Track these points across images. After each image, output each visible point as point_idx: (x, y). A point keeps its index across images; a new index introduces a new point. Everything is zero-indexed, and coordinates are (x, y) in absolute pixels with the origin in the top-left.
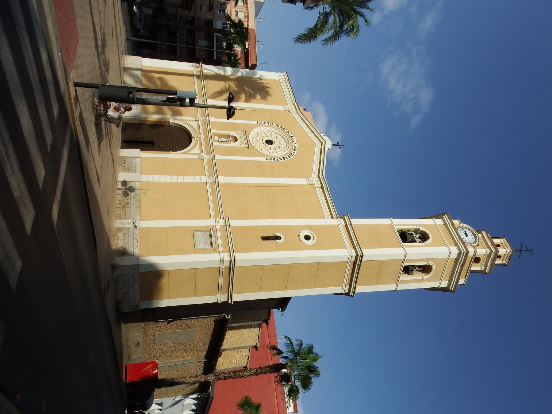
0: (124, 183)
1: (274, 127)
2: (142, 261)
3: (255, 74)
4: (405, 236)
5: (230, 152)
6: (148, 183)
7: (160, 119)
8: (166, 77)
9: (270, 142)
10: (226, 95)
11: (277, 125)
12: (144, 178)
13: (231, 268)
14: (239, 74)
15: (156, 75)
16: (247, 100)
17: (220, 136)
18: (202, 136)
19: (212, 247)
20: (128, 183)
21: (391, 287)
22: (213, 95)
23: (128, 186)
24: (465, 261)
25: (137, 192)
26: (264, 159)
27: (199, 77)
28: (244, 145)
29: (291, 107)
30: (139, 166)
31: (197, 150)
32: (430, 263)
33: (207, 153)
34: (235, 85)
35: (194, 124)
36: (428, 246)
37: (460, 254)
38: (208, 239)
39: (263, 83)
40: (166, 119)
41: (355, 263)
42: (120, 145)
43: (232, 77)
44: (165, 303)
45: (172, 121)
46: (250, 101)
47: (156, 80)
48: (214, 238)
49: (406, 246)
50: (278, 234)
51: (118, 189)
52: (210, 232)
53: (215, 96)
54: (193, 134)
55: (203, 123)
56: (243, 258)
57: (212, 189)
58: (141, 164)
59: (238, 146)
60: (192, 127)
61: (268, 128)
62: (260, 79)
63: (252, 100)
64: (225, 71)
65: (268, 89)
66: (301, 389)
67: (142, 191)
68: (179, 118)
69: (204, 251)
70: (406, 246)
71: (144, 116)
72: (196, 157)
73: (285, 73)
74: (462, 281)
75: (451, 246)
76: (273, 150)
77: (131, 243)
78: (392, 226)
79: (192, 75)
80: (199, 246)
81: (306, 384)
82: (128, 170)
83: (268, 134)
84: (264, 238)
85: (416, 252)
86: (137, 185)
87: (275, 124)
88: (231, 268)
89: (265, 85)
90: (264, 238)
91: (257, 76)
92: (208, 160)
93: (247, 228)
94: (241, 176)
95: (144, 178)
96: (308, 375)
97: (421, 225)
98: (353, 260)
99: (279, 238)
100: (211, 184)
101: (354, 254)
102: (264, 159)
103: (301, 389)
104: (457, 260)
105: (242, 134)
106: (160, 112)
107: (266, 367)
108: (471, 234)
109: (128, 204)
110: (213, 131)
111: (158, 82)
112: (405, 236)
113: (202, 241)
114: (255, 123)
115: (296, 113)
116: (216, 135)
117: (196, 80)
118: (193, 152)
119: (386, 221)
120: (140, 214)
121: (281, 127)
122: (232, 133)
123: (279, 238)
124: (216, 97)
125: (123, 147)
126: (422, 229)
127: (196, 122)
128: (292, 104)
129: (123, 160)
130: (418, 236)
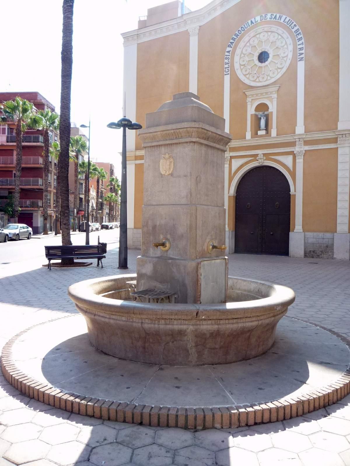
11: (229, 46)
31: (288, 160)
35: (236, 164)
59: (275, 103)
72: (300, 161)
114: (227, 79)
127: (233, 160)
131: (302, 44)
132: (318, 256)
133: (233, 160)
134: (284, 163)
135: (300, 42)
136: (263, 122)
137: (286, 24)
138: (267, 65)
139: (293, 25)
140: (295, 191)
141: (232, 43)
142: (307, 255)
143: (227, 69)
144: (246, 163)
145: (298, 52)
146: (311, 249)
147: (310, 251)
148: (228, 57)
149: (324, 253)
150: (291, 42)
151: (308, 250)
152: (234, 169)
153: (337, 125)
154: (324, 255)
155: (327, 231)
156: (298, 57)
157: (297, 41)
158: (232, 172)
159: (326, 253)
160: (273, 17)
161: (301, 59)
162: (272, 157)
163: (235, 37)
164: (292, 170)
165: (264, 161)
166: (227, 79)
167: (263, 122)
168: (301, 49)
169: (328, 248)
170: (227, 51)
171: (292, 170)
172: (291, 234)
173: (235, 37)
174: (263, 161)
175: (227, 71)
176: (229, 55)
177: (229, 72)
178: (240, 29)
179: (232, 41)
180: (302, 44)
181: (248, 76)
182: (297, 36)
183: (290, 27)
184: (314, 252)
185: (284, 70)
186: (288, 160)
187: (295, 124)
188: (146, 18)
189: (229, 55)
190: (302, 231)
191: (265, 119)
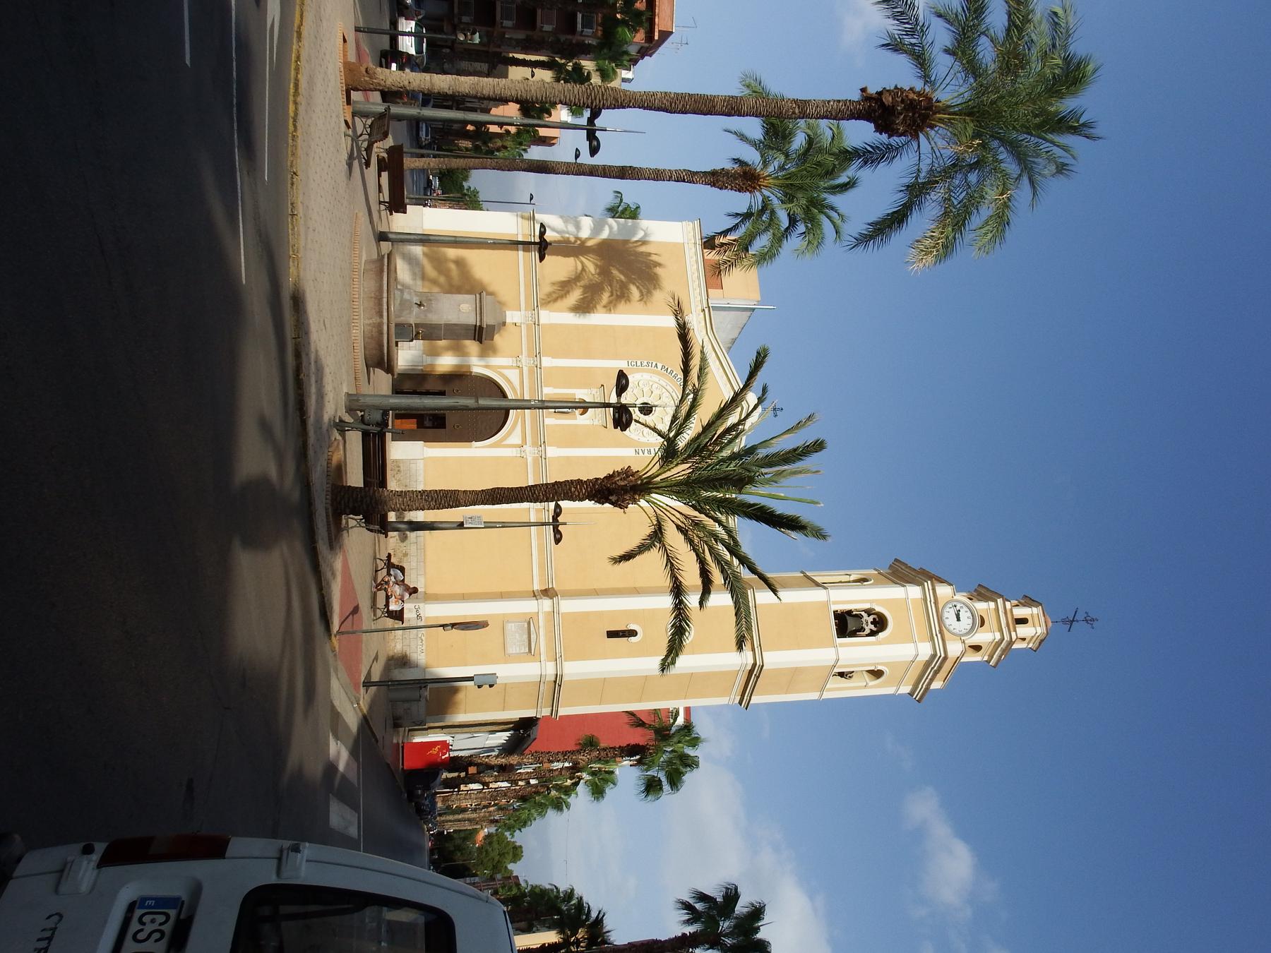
1: (659, 374)
2: (431, 673)
3: (634, 230)
4: (846, 624)
7: (456, 366)
10: (575, 296)
13: (557, 682)
14: (605, 234)
15: (452, 253)
16: (609, 307)
19: (530, 652)
21: (814, 696)
22: (549, 295)
24: (940, 668)
31: (516, 438)
32: (880, 668)
33: (534, 444)
34: (596, 265)
35: (513, 375)
36: (880, 643)
37: (934, 656)
38: (526, 636)
41: (751, 672)
43: (590, 243)
44: (461, 718)
47: (453, 266)
48: (533, 637)
49: (841, 645)
50: (632, 627)
52: (529, 622)
55: (531, 371)
56: (574, 669)
59: (587, 422)
60: (509, 381)
62: (643, 242)
63: (622, 306)
64: (578, 227)
65: (658, 270)
66: (666, 787)
69: (517, 659)
70: (841, 645)
71: (428, 360)
73: (697, 223)
74: (937, 685)
75: (922, 641)
77: (413, 647)
78: (827, 603)
80: (512, 650)
81: (675, 780)
83: (656, 392)
84: (611, 634)
85: (858, 652)
87: (660, 366)
88: (557, 682)
89: (654, 258)
90: (611, 634)
91: (640, 235)
92: (535, 460)
93: (586, 615)
94: (603, 358)
96: (678, 769)
97: (877, 601)
98: (749, 668)
99: (633, 633)
101: (751, 661)
103: (666, 787)
104: (928, 664)
106: (459, 351)
107: (614, 748)
108: (969, 614)
109: (406, 555)
112: (846, 624)
113: (516, 644)
118: (508, 442)
119: (817, 595)
120: (425, 574)
121: (671, 372)
123: (633, 633)
124: (555, 300)
126: (878, 609)
127: (517, 371)
128: (700, 308)
130: (871, 619)
133: (517, 371)
152: (506, 372)
186: (516, 438)
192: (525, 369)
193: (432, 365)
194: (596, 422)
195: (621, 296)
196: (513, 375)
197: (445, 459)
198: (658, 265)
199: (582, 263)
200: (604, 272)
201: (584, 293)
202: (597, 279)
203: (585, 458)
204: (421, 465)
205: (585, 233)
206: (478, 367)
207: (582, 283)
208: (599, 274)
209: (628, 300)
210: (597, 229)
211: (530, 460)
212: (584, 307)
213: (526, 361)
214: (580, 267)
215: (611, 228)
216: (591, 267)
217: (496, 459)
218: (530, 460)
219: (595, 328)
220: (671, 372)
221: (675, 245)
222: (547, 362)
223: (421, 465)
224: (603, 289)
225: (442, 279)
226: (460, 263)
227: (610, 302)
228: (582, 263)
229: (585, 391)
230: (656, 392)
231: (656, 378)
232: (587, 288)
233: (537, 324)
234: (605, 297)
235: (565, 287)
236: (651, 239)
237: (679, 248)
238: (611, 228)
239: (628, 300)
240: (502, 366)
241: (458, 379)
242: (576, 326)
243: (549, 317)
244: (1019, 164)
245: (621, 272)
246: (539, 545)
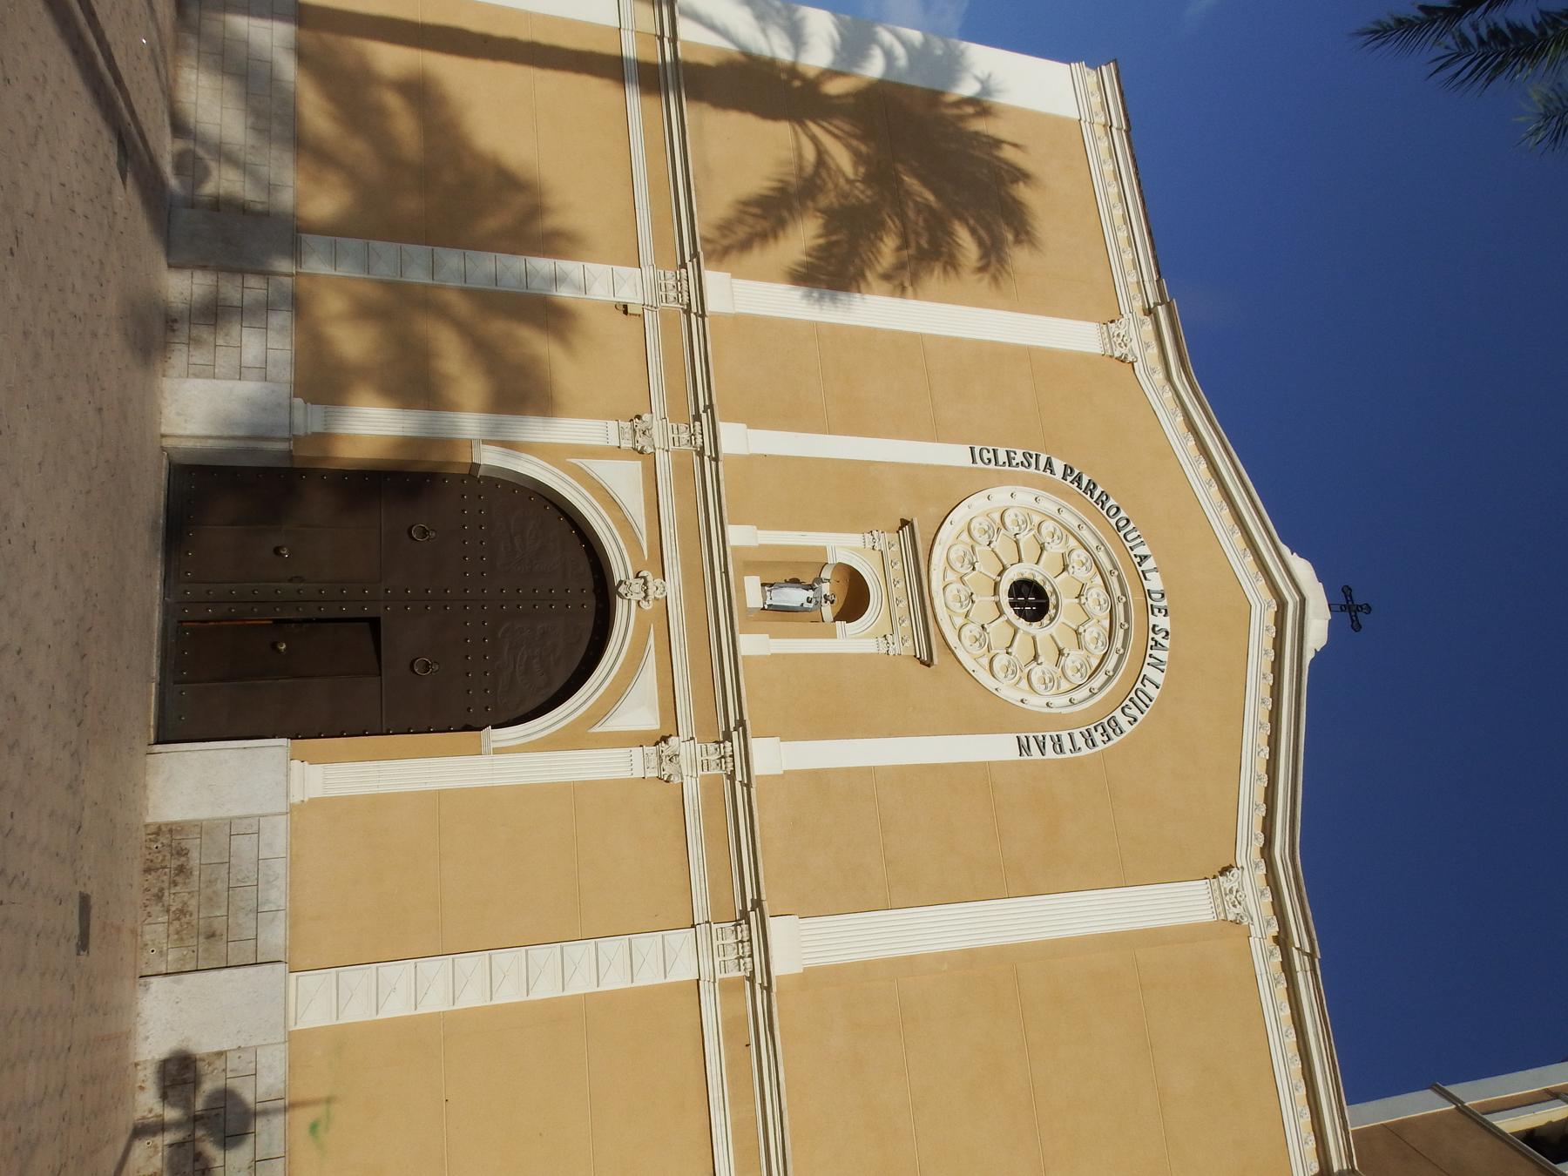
0: (180, 1072)
5: (831, 705)
6: (340, 1039)
7: (407, 442)
8: (450, 70)
9: (1031, 600)
10: (802, 237)
11: (1068, 470)
12: (326, 1000)
14: (874, 68)
15: (391, 58)
16: (903, 280)
17: (797, 571)
18: (672, 586)
20: (203, 1067)
22: (725, 227)
23: (208, 1086)
25: (269, 1133)
26: (999, 748)
27: (651, 79)
28: (904, 646)
29: (1139, 337)
30: (277, 896)
31: (639, 712)
33: (702, 733)
34: (858, 157)
35: (624, 479)
39: (997, 143)
40: (450, 443)
42: (142, 702)
43: (834, 87)
45: (490, 458)
46: (915, 279)
47: (393, 101)
51: (142, 1131)
53: (742, 232)
54: (620, 565)
57: (731, 1029)
58: (294, 861)
59: (869, 646)
60: (610, 502)
61: (1025, 496)
62: (980, 106)
63: (934, 280)
64: (796, 35)
65: (1023, 192)
67: (303, 1117)
68: (536, 430)
71: (309, 419)
72: (628, 764)
76: (1021, 649)
79: (608, 67)
82: (212, 946)
83: (1055, 549)
86: (265, 1080)
87: (1059, 466)
89: (1008, 153)
91: (967, 88)
92: (709, 786)
95: (326, 1000)
100: (728, 987)
102: (999, 748)
105: (889, 541)
110: (739, 536)
111: (404, 124)
114: (955, 455)
115: (1159, 376)
116: (751, 566)
117: (633, 97)
121: (1092, 485)
122: (845, 548)
124: (745, 246)
125: (179, 725)
127: (636, 466)
128: (1138, 304)
129: (172, 852)
131: (1075, 749)
132: (159, 897)
133: (636, 466)
134: (629, 692)
135: (1080, 741)
136: (795, 597)
137: (1139, 685)
138: (1002, 613)
139: (1134, 711)
140: (497, 751)
141: (1079, 479)
142: (164, 839)
143: (991, 455)
144: (624, 524)
145: (1048, 735)
146: (194, 854)
147: (182, 852)
148: (1033, 461)
149: (176, 924)
150: (1009, 489)
151: (192, 844)
152: (603, 470)
153: (737, 420)
154: (161, 928)
155: (294, 922)
156: (1031, 735)
157: (1083, 730)
158: (585, 461)
159: (178, 933)
160: (1159, 638)
161: (1023, 748)
162: (651, 641)
163: (1097, 493)
164: (596, 729)
165: (634, 604)
166: (955, 455)
167: (795, 597)
168: (1058, 744)
169: (202, 939)
170: (1054, 460)
171: (596, 729)
172: (278, 747)
173: (1097, 493)
174: (635, 598)
175: (986, 455)
176: (1037, 467)
177: (980, 464)
178: (1123, 514)
179: (1162, 655)
180: (1075, 749)
181: (965, 536)
182: (1100, 730)
183: (1127, 702)
184: (181, 870)
185: (983, 677)
186: (639, 712)
187: (788, 735)
188: (1108, 71)
189: (1037, 467)
190: (296, 798)
191: (806, 605)
192: (662, 458)
193: (324, 438)
194: (896, 648)
195: (924, 260)
196: (624, 479)
197: (378, 803)
198: (1022, 175)
199: (814, 140)
200: (879, 174)
201: (828, 229)
202: (862, 193)
203: (869, 773)
204: (277, 840)
205: (818, 56)
206: (479, 438)
207: (828, 199)
208: (868, 180)
209: (951, 263)
210: (853, 45)
211: (692, 789)
212: (830, 272)
213: (664, 434)
214: (810, 154)
215: (889, 56)
216: (842, 158)
217: (575, 792)
218: (692, 789)
219: (868, 336)
220: (1092, 485)
221: (1059, 123)
222: (735, 439)
223: (277, 840)
224: (882, 225)
225: (357, 148)
226: (419, 92)
227: (900, 266)
228: (814, 140)
229: (855, 539)
230: (1055, 549)
231: (1049, 504)
232: (835, 219)
233: (695, 309)
234: (888, 246)
235: (766, 214)
236: (1001, 99)
237: (1066, 132)
238: (889, 56)
239: (951, 263)
240: (582, 453)
241: (408, 485)
242: (816, 326)
243: (736, 293)
244: (981, 258)
245: (925, 182)
246: (740, 1131)
